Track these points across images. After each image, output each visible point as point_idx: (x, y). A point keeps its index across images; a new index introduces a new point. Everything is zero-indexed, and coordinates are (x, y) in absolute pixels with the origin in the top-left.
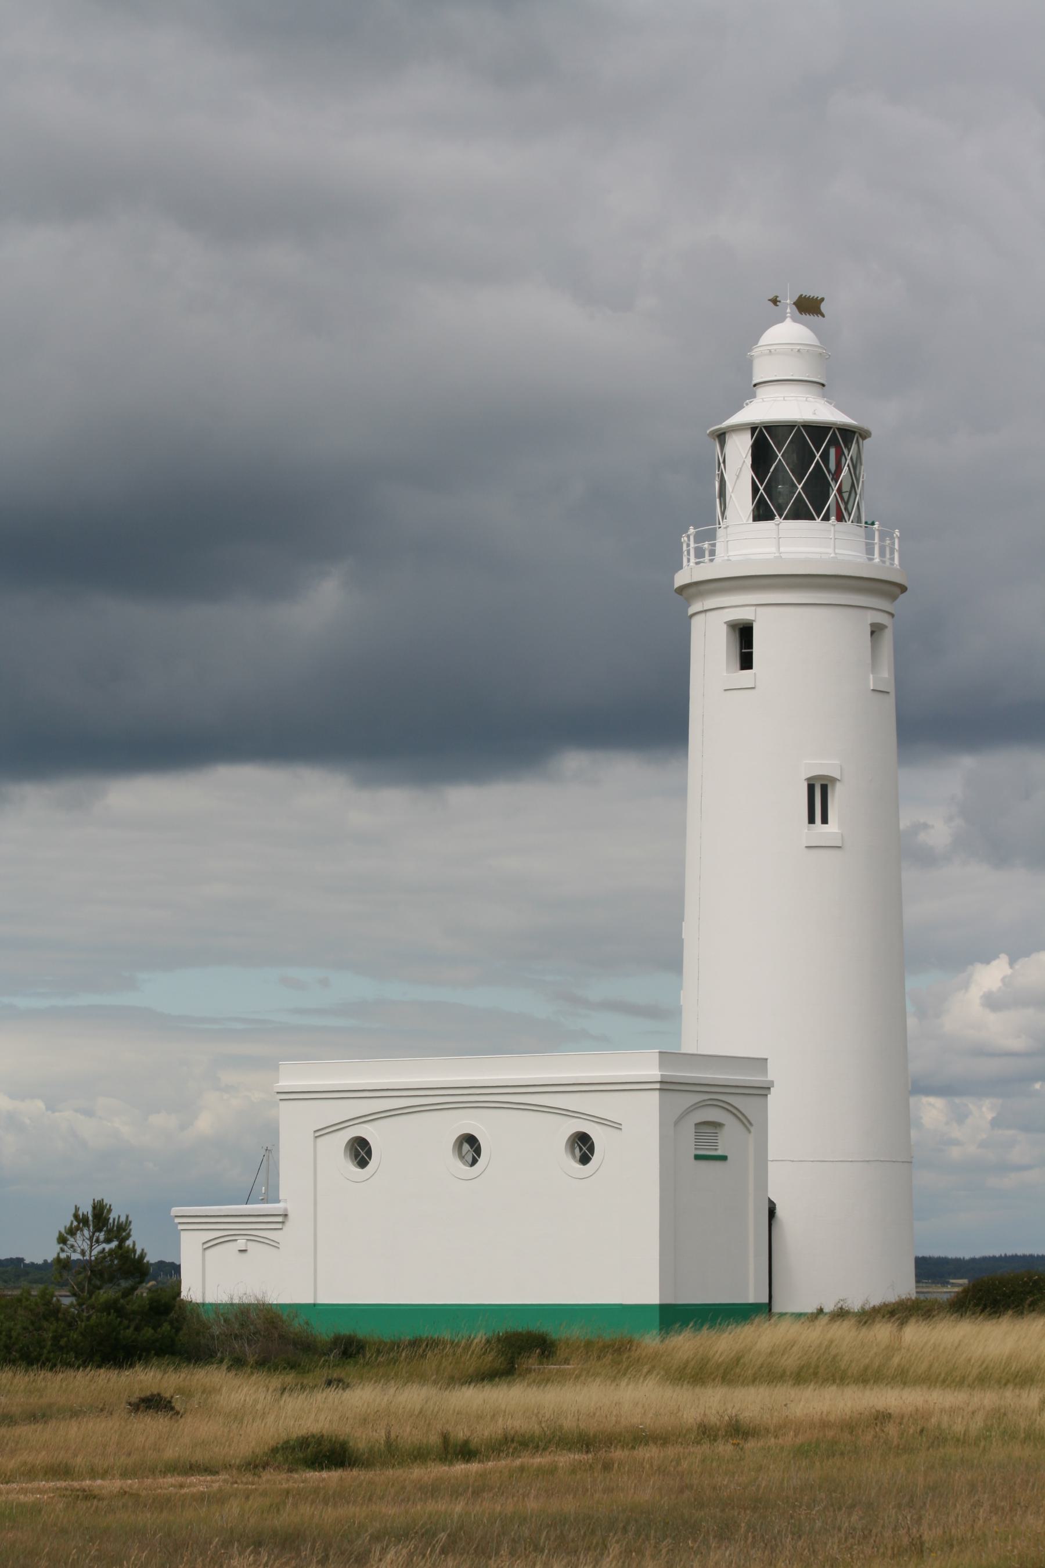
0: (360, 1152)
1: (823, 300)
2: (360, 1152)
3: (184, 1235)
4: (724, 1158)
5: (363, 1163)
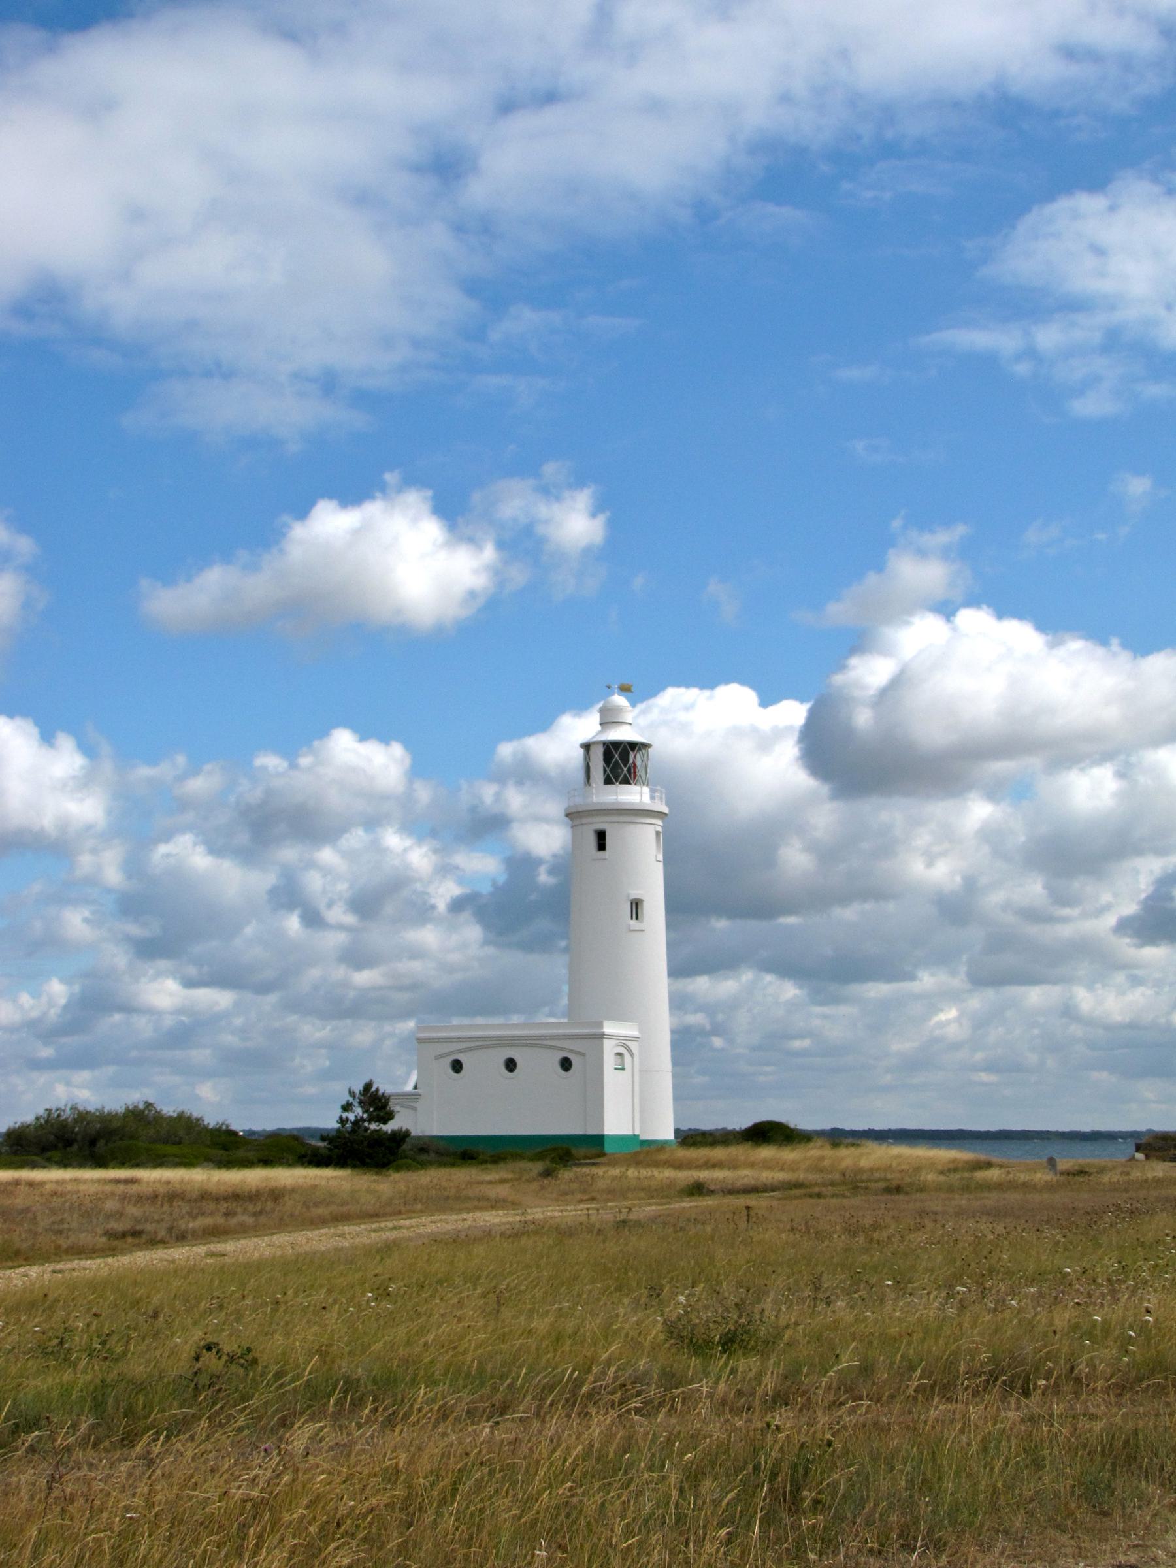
0: (457, 1066)
2: (457, 1066)
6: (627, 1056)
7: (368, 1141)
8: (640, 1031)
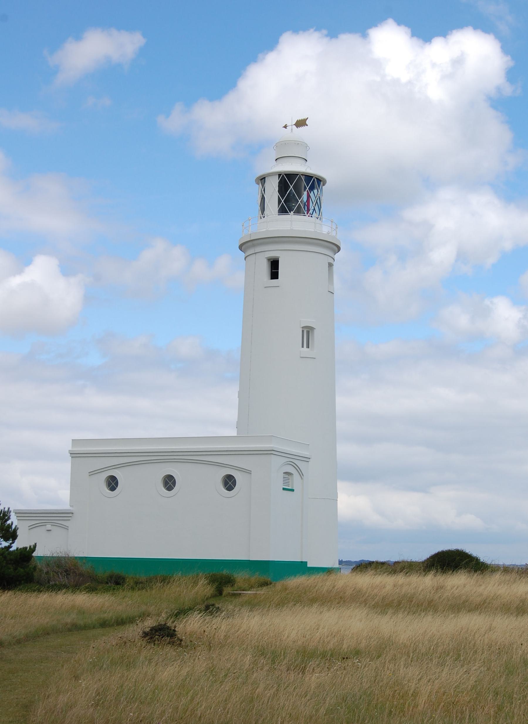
0: (112, 483)
1: (307, 125)
2: (112, 483)
3: (341, 485)
4: (292, 490)
5: (113, 489)
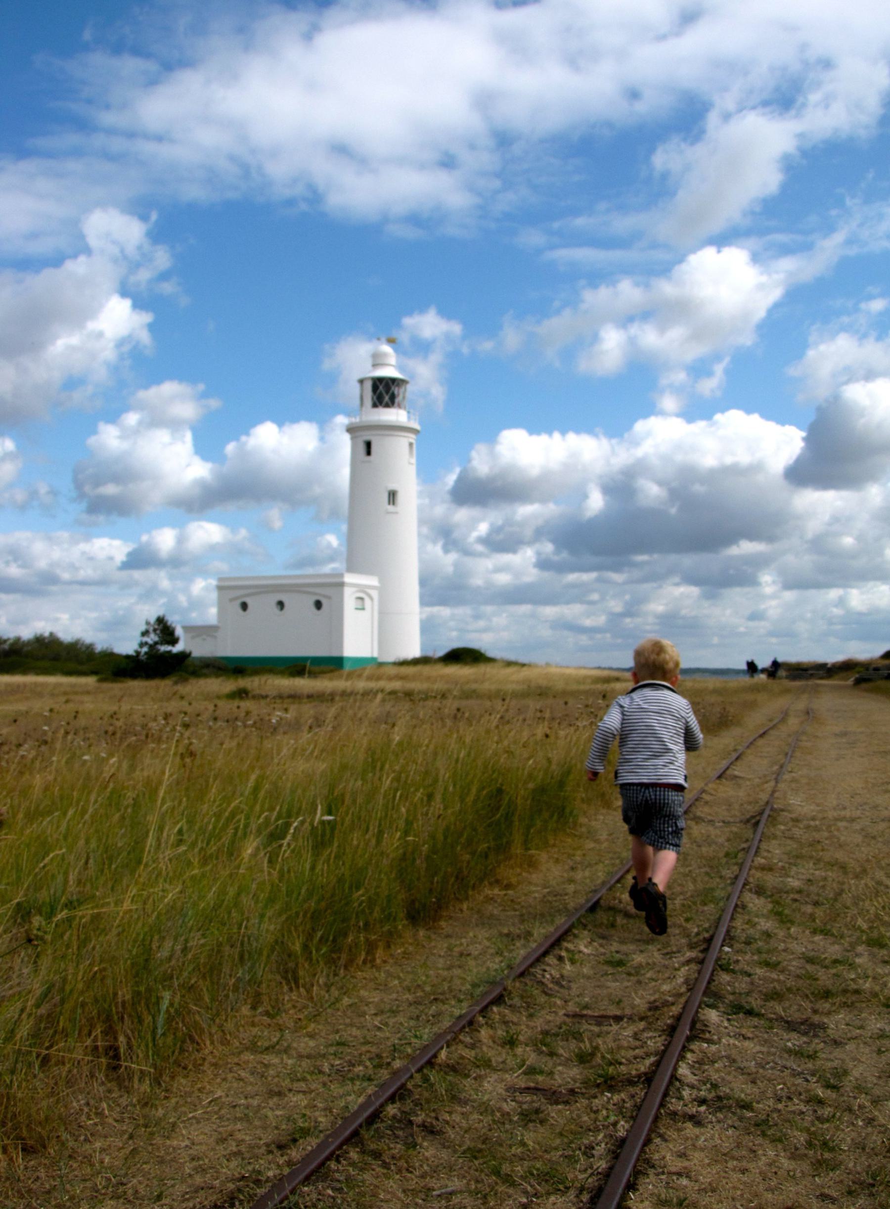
0: (244, 606)
2: (244, 606)
6: (367, 601)
7: (161, 661)
8: (380, 581)
